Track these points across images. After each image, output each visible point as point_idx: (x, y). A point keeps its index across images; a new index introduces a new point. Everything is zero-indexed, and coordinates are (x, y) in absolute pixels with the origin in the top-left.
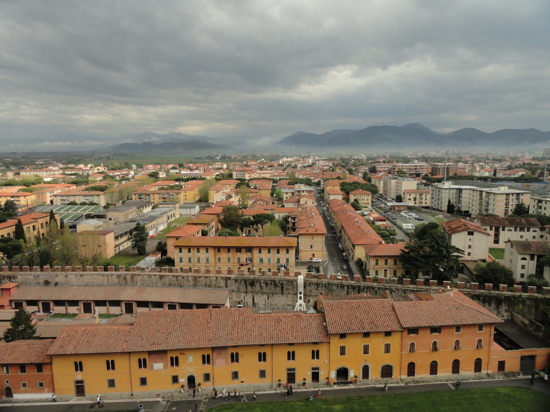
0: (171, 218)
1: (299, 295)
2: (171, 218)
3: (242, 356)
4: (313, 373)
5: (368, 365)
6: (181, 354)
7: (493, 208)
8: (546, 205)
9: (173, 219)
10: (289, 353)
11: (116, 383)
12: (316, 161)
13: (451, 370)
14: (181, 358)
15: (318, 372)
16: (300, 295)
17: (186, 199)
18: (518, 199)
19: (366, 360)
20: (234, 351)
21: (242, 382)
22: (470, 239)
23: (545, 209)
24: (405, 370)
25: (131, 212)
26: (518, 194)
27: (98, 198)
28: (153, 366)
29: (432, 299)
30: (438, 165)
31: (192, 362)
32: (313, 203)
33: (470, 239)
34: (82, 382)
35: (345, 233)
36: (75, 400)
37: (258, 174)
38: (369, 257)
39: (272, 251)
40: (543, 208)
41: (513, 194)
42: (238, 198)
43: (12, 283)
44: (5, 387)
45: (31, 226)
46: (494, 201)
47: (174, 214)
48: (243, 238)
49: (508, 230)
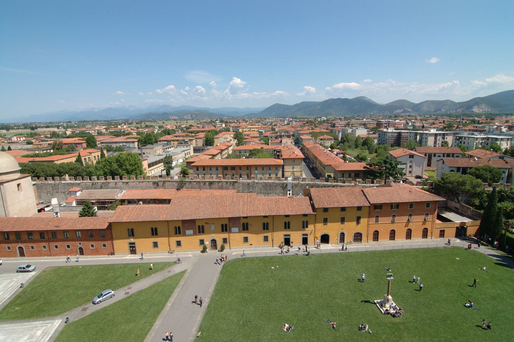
0: (188, 155)
1: (288, 192)
2: (188, 155)
3: (251, 225)
4: (303, 238)
5: (343, 232)
6: (206, 223)
7: (426, 140)
8: (465, 140)
9: (189, 156)
10: (285, 223)
11: (159, 245)
12: (290, 122)
13: (405, 236)
14: (206, 226)
15: (307, 238)
16: (290, 192)
17: (197, 145)
18: (443, 138)
19: (342, 229)
20: (245, 221)
21: (251, 245)
22: (411, 161)
23: (464, 143)
24: (371, 236)
25: (158, 149)
26: (444, 134)
27: (133, 144)
28: (185, 232)
29: (391, 186)
30: (381, 121)
31: (214, 230)
32: (291, 143)
33: (411, 161)
34: (134, 243)
35: (317, 160)
36: (130, 257)
37: (248, 128)
38: (337, 172)
39: (265, 169)
40: (463, 143)
41: (440, 134)
42: (236, 141)
43: (78, 188)
44: (79, 247)
45: (87, 157)
46: (425, 143)
47: (189, 152)
48: (243, 159)
49: (438, 156)
